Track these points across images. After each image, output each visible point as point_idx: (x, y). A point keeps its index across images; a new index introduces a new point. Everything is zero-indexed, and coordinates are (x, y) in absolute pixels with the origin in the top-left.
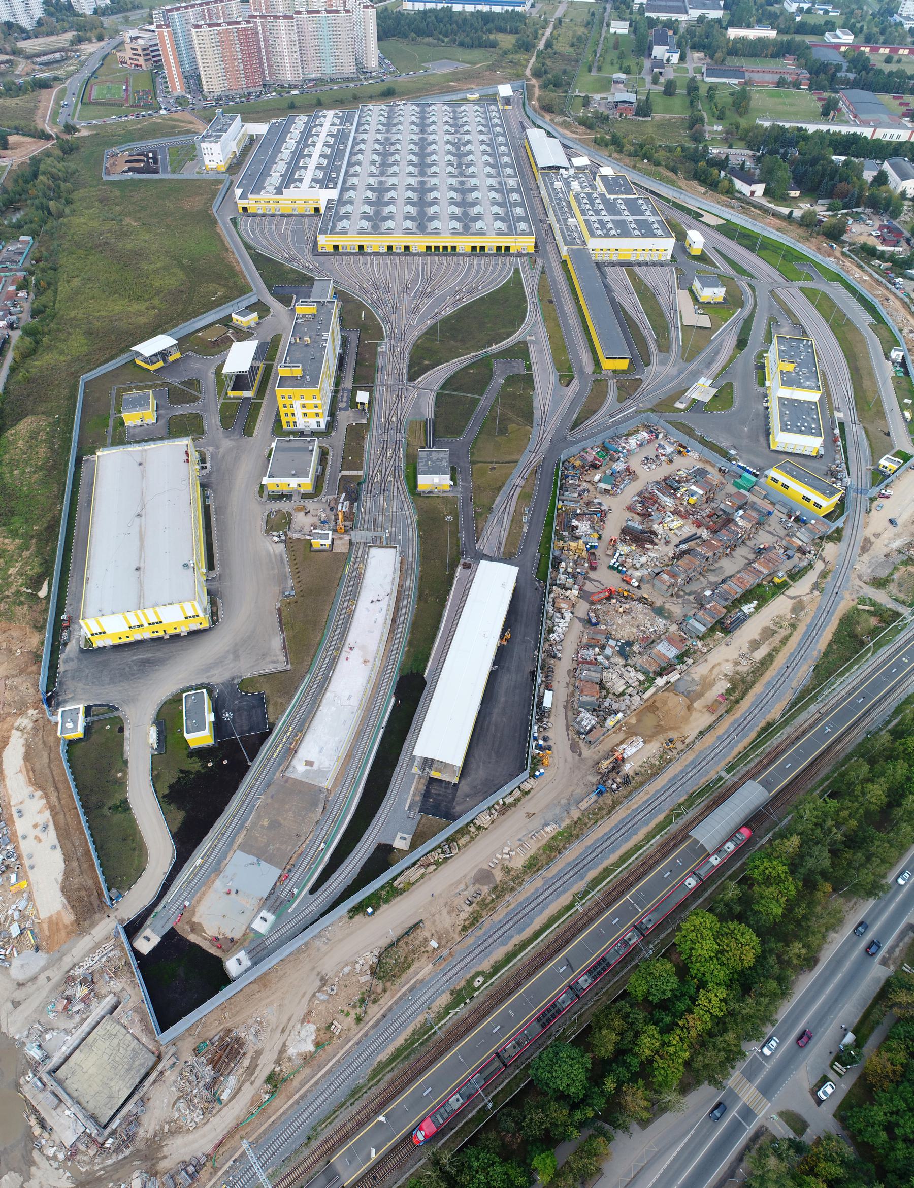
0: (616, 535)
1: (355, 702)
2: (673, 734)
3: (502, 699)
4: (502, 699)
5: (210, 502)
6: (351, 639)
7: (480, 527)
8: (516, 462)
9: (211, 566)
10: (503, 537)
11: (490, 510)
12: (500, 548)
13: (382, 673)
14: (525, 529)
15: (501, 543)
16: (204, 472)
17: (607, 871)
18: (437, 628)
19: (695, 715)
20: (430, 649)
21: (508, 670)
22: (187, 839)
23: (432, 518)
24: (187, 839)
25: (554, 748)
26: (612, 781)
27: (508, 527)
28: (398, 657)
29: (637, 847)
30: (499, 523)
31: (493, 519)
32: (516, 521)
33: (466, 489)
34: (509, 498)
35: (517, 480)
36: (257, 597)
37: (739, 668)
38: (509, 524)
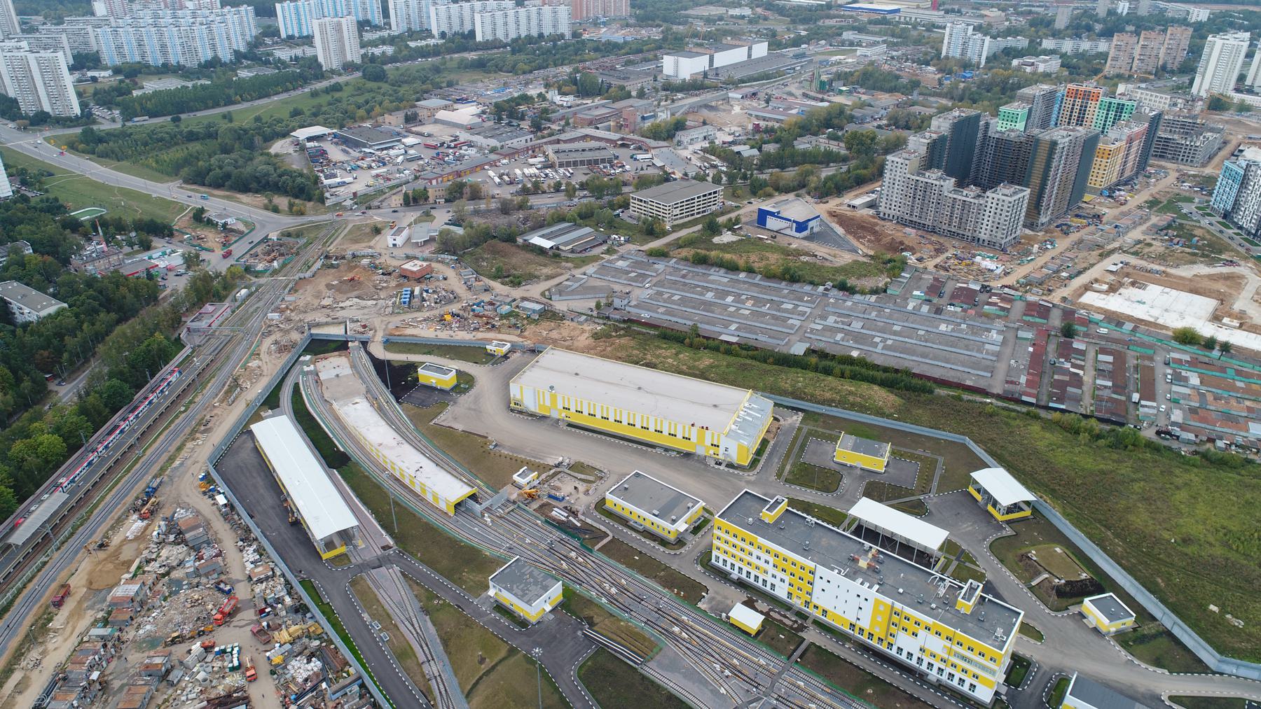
0: (254, 691)
1: (363, 431)
2: (102, 555)
3: (262, 491)
4: (262, 491)
5: (659, 451)
6: (407, 447)
7: (415, 586)
8: (468, 695)
9: (570, 425)
10: (381, 595)
11: (426, 610)
12: (373, 582)
13: (367, 455)
14: (366, 616)
15: (378, 588)
16: (712, 464)
17: (128, 471)
18: (358, 496)
19: (84, 582)
20: (348, 483)
21: (273, 508)
22: (379, 365)
23: (469, 563)
24: (379, 365)
25: (201, 496)
26: (147, 505)
27: (386, 607)
28: (366, 465)
29: (110, 490)
30: (401, 605)
31: (412, 607)
32: (385, 618)
33: (481, 615)
34: (422, 640)
35: (436, 667)
36: (504, 431)
37: (41, 650)
38: (390, 612)
